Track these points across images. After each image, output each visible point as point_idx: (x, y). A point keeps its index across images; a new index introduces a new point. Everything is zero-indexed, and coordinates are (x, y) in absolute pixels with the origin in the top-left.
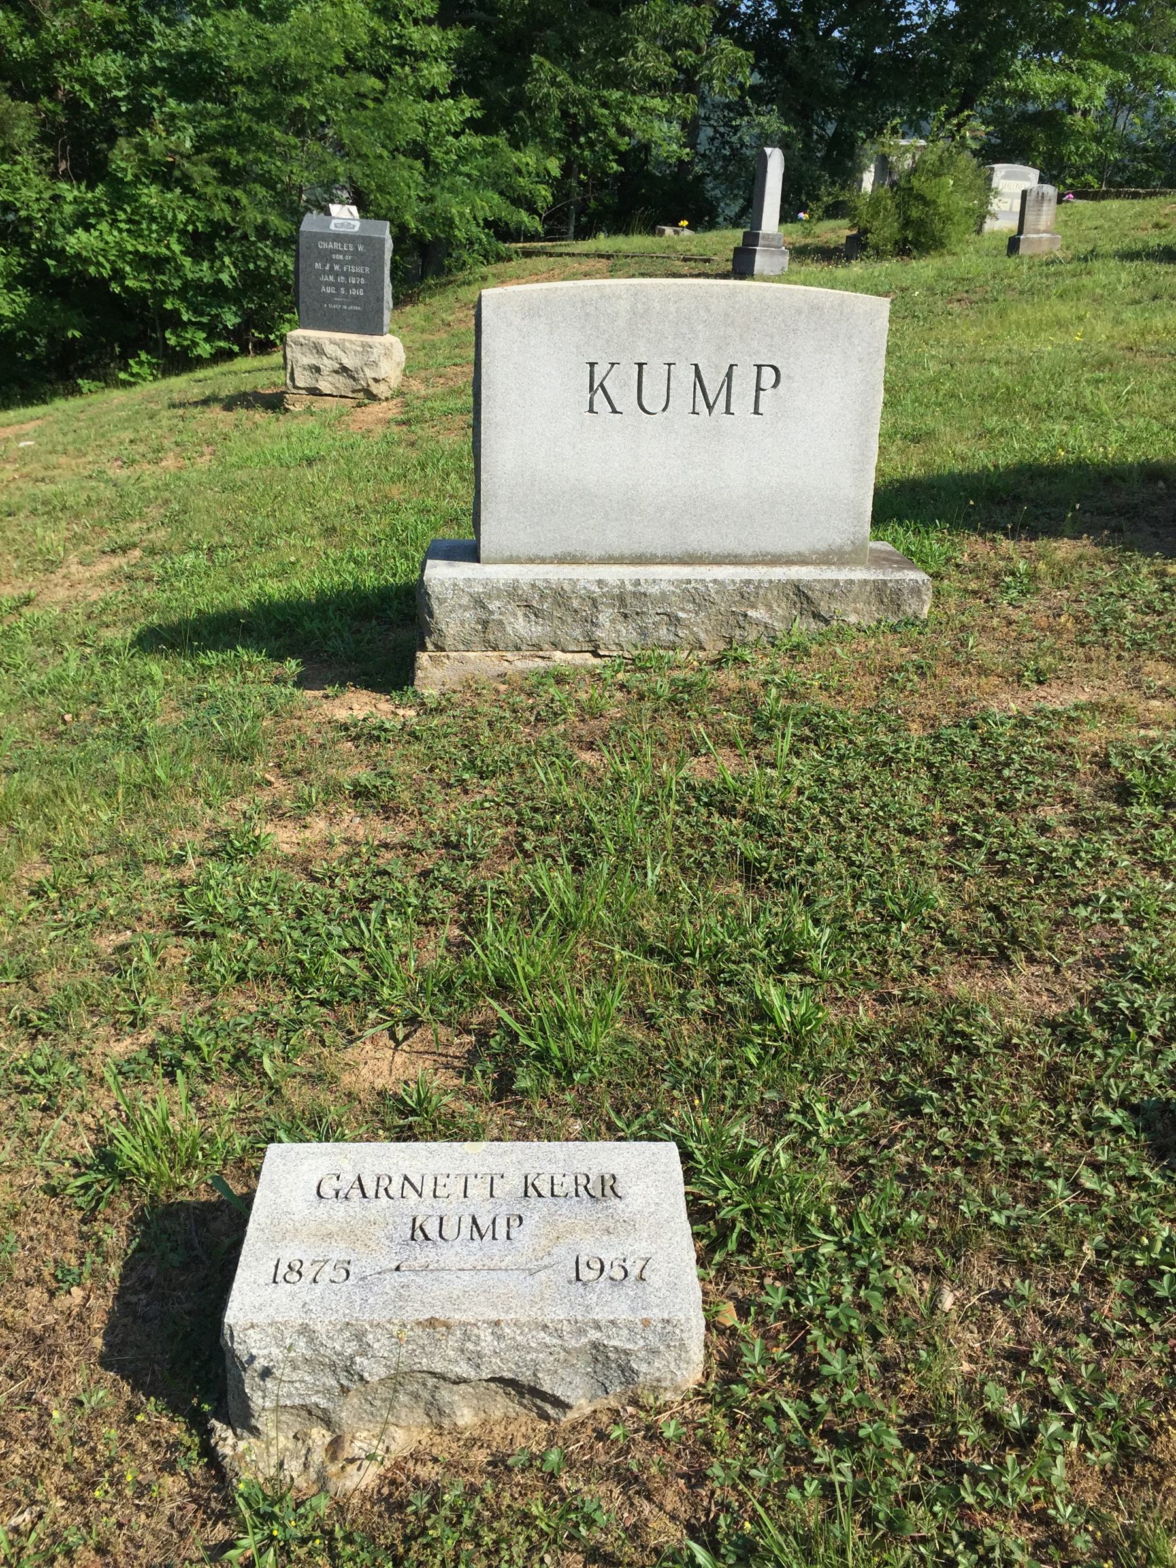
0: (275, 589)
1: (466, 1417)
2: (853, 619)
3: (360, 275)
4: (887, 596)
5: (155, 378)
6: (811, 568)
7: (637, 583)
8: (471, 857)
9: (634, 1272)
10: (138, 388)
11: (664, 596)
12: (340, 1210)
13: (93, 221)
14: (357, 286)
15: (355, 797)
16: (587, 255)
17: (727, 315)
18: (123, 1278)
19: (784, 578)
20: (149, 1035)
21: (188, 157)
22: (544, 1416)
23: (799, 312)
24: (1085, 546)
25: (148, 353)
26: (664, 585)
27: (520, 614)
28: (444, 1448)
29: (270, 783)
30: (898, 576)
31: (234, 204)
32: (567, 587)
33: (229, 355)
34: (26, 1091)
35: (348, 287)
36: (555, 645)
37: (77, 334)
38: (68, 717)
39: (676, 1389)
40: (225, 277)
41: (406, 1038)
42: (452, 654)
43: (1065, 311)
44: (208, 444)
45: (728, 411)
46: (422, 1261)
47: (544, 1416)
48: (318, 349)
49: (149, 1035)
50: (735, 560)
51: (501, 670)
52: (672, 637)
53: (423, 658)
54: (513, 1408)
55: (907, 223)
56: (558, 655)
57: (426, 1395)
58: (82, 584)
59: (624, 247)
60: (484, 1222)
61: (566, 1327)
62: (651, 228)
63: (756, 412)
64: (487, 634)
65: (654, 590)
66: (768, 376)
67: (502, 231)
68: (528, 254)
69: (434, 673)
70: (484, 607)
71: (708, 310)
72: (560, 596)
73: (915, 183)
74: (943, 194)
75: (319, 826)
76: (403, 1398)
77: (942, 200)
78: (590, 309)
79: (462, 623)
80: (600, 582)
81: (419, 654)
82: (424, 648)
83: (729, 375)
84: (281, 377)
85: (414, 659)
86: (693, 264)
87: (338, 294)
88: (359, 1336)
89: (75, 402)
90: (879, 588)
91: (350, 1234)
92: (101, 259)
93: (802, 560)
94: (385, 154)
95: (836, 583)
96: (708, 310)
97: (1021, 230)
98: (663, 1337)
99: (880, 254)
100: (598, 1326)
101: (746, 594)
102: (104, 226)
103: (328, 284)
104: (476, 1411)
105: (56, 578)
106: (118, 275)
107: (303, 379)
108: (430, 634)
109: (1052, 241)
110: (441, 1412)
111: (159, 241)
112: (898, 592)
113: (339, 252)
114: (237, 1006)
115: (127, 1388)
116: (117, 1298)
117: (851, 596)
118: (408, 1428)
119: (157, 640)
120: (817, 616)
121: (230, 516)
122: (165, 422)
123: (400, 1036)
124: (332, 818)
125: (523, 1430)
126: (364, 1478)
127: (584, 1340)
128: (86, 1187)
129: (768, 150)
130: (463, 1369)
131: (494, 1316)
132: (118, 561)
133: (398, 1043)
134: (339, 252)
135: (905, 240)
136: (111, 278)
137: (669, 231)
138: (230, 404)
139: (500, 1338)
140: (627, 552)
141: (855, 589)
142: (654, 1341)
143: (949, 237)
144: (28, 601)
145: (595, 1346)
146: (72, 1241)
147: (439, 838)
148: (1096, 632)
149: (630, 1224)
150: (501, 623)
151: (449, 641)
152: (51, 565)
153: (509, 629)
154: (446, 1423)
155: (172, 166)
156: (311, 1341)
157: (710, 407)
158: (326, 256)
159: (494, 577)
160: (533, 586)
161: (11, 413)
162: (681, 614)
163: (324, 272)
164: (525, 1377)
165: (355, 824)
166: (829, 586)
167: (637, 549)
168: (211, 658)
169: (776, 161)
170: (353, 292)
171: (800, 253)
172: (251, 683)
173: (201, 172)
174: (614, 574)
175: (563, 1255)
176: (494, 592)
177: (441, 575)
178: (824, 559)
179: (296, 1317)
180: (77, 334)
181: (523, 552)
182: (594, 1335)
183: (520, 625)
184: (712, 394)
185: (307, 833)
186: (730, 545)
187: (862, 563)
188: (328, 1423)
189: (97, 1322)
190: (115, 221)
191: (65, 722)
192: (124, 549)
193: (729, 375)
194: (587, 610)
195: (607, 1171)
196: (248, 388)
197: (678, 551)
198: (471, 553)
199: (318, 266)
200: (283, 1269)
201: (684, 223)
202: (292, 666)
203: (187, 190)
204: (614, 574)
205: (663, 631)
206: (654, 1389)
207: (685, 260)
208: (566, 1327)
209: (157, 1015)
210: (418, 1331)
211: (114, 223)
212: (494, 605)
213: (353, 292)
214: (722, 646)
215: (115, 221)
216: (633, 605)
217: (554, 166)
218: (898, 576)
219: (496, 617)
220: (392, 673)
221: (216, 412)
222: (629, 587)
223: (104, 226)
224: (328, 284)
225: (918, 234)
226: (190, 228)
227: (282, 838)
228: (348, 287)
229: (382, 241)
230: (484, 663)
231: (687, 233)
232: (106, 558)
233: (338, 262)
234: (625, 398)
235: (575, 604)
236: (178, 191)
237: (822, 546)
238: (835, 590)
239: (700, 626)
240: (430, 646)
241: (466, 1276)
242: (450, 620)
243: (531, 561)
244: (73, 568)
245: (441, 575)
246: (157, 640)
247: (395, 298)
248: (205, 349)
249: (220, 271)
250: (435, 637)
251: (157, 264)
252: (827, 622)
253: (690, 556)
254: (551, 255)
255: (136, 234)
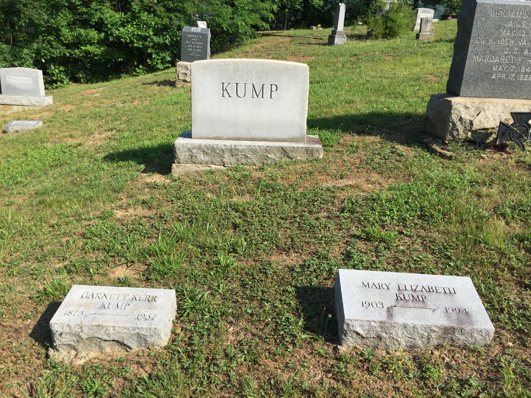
0: (147, 143)
1: (108, 350)
2: (299, 158)
3: (200, 45)
4: (309, 152)
5: (145, 74)
6: (288, 143)
7: (236, 146)
8: (165, 221)
9: (152, 317)
10: (137, 78)
11: (243, 150)
12: (86, 300)
13: (126, 24)
14: (199, 49)
15: (143, 204)
16: (285, 36)
17: (261, 70)
18: (41, 318)
19: (278, 146)
20: (66, 263)
21: (156, 4)
22: (127, 351)
23: (282, 70)
24: (377, 139)
25: (143, 66)
26: (243, 147)
27: (202, 154)
28: (102, 356)
29: (122, 199)
30: (313, 146)
31: (170, 19)
32: (215, 147)
33: (168, 67)
34: (32, 275)
35: (196, 48)
36: (212, 163)
37: (122, 60)
38: (78, 179)
39: (158, 346)
40: (167, 42)
41: (130, 266)
42: (182, 165)
43: (420, 60)
44: (149, 97)
45: (263, 97)
46: (101, 312)
47: (127, 351)
48: (186, 68)
49: (66, 263)
50: (266, 140)
51: (196, 170)
52: (246, 162)
53: (174, 165)
54: (120, 349)
55: (387, 28)
56: (213, 166)
57: (98, 344)
58: (98, 141)
59: (297, 34)
60: (119, 305)
61: (131, 328)
62: (308, 27)
63: (271, 98)
64: (192, 159)
65: (240, 148)
66: (274, 88)
67: (256, 27)
68: (264, 35)
69: (177, 170)
70: (191, 151)
71: (256, 69)
72: (213, 149)
73: (390, 15)
74: (399, 18)
75: (131, 211)
76: (93, 344)
77: (398, 20)
78: (222, 68)
79: (185, 156)
80: (225, 145)
81: (173, 164)
82: (174, 163)
83: (263, 87)
84: (174, 75)
85: (172, 166)
86: (316, 40)
87: (193, 51)
88: (81, 327)
89: (119, 81)
90: (307, 149)
91: (86, 306)
92: (126, 36)
93: (286, 140)
94: (219, 3)
95: (294, 148)
96: (256, 69)
97: (420, 32)
98: (154, 332)
99: (376, 38)
100: (138, 329)
101: (268, 150)
102: (129, 26)
103: (190, 48)
104: (111, 349)
105: (91, 138)
106: (132, 42)
107: (181, 77)
108: (176, 159)
109: (430, 35)
110: (102, 349)
111: (146, 31)
112: (312, 151)
113: (193, 38)
114: (92, 256)
115: (34, 341)
116: (38, 322)
117: (298, 151)
118: (95, 352)
119: (111, 158)
120: (288, 157)
121: (144, 120)
122: (139, 89)
123: (129, 265)
124: (135, 209)
125: (119, 353)
126: (81, 362)
127: (135, 332)
128: (38, 297)
129: (340, 4)
130: (106, 338)
131: (114, 325)
132: (109, 134)
133: (128, 267)
134: (193, 38)
135: (386, 33)
136: (130, 43)
137: (314, 28)
138: (160, 84)
139: (115, 330)
140: (234, 137)
141: (300, 149)
142: (152, 333)
143: (400, 32)
144: (80, 145)
145: (138, 333)
146: (32, 309)
147: (159, 215)
148: (367, 165)
149: (155, 307)
150: (196, 156)
151: (181, 161)
152: (91, 134)
153: (199, 158)
154: (103, 351)
155: (151, 7)
156: (70, 328)
157: (257, 96)
158: (190, 39)
159: (194, 143)
160: (205, 146)
161: (99, 84)
162: (248, 155)
163: (189, 44)
164: (121, 340)
165: (141, 211)
166: (292, 149)
167: (238, 136)
168: (121, 163)
169: (343, 8)
170: (198, 50)
171: (351, 37)
172: (132, 170)
173: (160, 9)
174: (229, 143)
175: (136, 313)
176: (194, 147)
177: (180, 142)
178: (292, 140)
179: (67, 322)
180: (122, 60)
181: (204, 136)
182: (137, 331)
183: (202, 157)
184: (258, 92)
185: (127, 213)
186: (264, 136)
187: (304, 142)
188: (75, 349)
189: (32, 327)
190: (133, 25)
191: (77, 181)
192: (112, 130)
193: (263, 87)
194: (221, 153)
195: (154, 295)
196: (167, 79)
197: (249, 137)
198: (188, 135)
199: (187, 42)
200: (68, 312)
201: (320, 25)
202: (142, 167)
203: (156, 15)
204: (229, 143)
205: (243, 160)
206: (153, 345)
207: (315, 38)
208: (131, 328)
209: (70, 258)
210: (95, 327)
211: (132, 25)
212: (194, 151)
213: (198, 50)
214: (261, 165)
215: (133, 25)
216: (235, 152)
217: (275, 7)
218: (313, 146)
219: (194, 154)
220: (165, 169)
221: (155, 87)
222: (233, 147)
223: (129, 26)
224: (190, 48)
225: (390, 31)
226: (156, 26)
227: (119, 214)
228: (196, 48)
229: (207, 35)
230: (192, 167)
231: (321, 29)
232: (107, 132)
233: (193, 41)
234: (233, 93)
235: (218, 151)
236: (152, 15)
237: (292, 137)
238: (293, 149)
239: (254, 159)
240: (176, 162)
241: (110, 316)
242: (181, 155)
243: (207, 138)
244: (96, 135)
245: (180, 142)
246: (111, 158)
247: (346, 19)
248: (160, 66)
249: (166, 39)
250: (177, 159)
251: (145, 38)
252: (292, 159)
253: (253, 138)
254: (274, 36)
255: (139, 29)
